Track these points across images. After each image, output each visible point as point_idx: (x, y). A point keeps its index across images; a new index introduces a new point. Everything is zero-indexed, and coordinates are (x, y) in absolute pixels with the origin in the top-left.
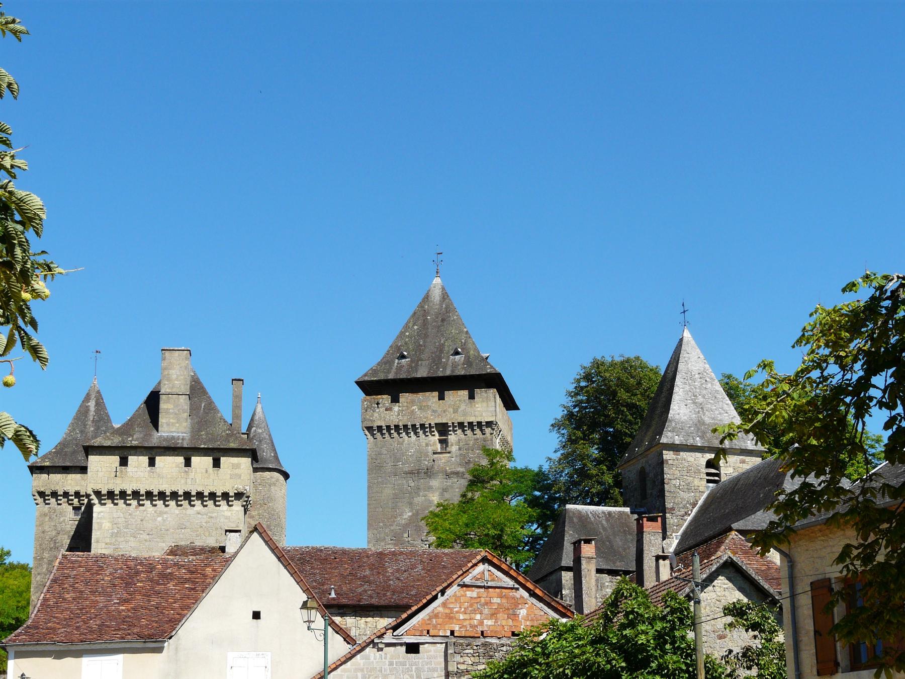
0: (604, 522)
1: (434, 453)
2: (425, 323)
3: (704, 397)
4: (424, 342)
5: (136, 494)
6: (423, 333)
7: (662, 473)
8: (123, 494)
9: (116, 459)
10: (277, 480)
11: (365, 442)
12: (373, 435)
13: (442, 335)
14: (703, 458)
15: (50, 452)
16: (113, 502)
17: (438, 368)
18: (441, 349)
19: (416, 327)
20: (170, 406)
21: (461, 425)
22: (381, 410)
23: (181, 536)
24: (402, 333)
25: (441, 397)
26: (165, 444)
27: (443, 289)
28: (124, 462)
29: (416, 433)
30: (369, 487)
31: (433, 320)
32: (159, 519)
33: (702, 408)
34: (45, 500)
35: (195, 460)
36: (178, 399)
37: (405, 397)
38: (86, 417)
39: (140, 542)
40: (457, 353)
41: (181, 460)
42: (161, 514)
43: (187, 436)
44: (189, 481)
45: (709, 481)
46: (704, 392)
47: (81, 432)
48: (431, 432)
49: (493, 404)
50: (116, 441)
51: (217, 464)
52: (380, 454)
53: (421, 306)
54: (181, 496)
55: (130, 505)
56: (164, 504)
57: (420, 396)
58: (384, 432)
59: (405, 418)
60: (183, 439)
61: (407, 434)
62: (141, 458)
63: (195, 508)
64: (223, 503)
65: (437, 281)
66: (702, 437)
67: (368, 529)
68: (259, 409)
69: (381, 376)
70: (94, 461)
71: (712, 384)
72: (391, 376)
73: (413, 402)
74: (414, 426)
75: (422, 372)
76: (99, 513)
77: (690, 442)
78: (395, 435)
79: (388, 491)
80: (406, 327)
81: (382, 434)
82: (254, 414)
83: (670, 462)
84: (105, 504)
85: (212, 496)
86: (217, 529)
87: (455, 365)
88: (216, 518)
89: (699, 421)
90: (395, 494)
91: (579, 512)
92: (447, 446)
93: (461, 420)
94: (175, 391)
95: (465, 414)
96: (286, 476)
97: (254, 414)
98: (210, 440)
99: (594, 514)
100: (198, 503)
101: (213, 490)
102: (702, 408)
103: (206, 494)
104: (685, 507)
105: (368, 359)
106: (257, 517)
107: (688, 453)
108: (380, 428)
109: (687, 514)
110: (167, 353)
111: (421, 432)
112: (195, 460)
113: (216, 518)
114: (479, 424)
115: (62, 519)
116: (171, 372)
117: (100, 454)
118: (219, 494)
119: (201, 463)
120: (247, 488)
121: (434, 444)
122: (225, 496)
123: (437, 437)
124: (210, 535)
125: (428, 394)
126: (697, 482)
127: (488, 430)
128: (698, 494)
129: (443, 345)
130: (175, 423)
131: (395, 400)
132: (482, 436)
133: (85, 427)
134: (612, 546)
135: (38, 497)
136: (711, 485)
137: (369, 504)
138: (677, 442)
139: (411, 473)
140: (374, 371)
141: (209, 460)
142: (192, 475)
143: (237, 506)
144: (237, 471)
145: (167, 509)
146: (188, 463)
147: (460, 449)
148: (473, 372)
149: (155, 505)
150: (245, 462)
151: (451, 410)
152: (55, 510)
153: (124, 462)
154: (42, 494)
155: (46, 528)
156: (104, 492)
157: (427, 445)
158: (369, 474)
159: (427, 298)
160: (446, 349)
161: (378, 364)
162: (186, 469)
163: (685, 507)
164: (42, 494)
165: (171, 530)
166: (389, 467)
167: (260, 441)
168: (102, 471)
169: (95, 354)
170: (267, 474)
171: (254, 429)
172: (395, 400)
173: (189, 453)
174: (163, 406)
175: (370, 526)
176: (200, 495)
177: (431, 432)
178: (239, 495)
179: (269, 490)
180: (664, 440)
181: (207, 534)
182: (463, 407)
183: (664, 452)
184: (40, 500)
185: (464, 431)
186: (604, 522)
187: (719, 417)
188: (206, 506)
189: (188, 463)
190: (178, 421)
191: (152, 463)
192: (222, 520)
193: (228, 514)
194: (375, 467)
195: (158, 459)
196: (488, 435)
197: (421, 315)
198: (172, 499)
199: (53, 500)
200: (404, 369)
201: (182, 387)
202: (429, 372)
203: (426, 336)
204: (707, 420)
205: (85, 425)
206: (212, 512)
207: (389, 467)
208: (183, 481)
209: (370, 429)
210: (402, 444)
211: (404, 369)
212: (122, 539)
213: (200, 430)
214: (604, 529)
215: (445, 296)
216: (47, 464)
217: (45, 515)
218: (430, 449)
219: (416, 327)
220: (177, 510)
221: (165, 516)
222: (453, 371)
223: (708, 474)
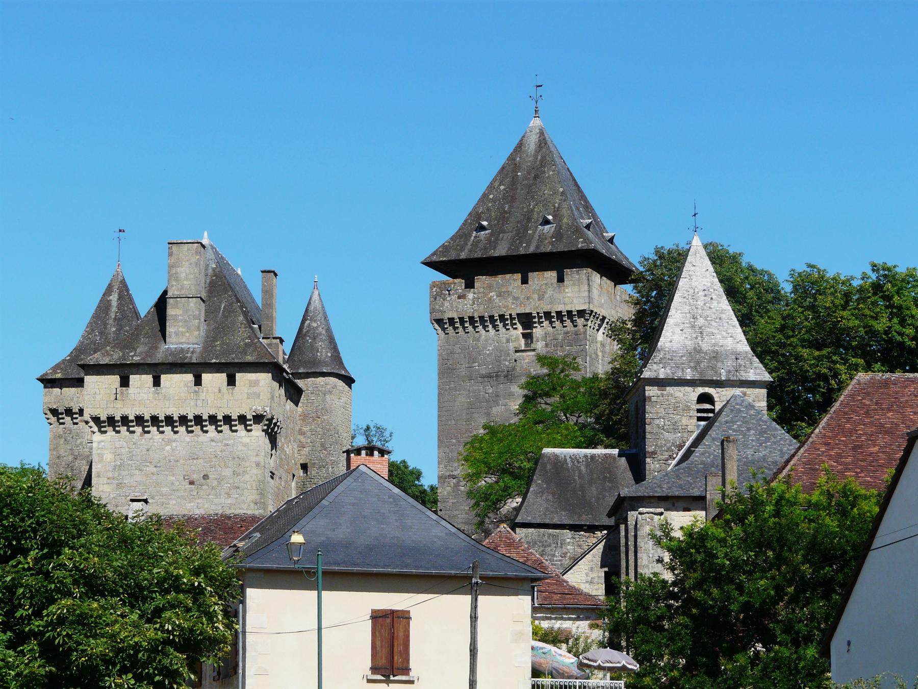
0: (583, 468)
1: (516, 351)
2: (514, 181)
3: (706, 318)
4: (511, 207)
5: (140, 420)
6: (510, 197)
7: (644, 412)
8: (125, 420)
9: (115, 379)
10: (335, 387)
11: (432, 338)
12: (444, 329)
13: (533, 197)
14: (693, 393)
15: (64, 360)
16: (114, 430)
17: (521, 243)
18: (528, 218)
19: (502, 187)
20: (179, 312)
21: (548, 315)
22: (453, 297)
23: (193, 468)
24: (485, 196)
25: (525, 281)
26: (170, 359)
27: (542, 133)
28: (125, 383)
29: (495, 327)
30: (440, 394)
31: (529, 174)
32: (168, 448)
33: (701, 333)
34: (58, 419)
35: (206, 377)
36: (188, 303)
37: (481, 281)
38: (107, 314)
39: (147, 475)
40: (546, 222)
41: (190, 377)
42: (170, 441)
43: (198, 348)
44: (200, 403)
45: (699, 419)
46: (708, 312)
47: (101, 333)
48: (513, 324)
49: (586, 287)
50: (115, 357)
51: (231, 381)
52: (452, 353)
53: (511, 158)
54: (191, 421)
55: (133, 432)
56: (173, 430)
57: (499, 279)
58: (458, 325)
59: (482, 308)
60: (193, 352)
61: (485, 327)
62: (144, 376)
63: (208, 435)
64: (240, 428)
65: (536, 123)
66: (694, 368)
67: (439, 447)
68: (316, 297)
69: (452, 256)
70: (90, 380)
71: (719, 303)
72: (463, 255)
73: (490, 287)
74: (491, 317)
75: (501, 250)
76: (99, 442)
77: (679, 374)
78: (470, 329)
79: (462, 399)
80: (491, 188)
81: (455, 328)
82: (309, 303)
83: (654, 399)
84: (105, 432)
85: (227, 419)
86: (234, 458)
87: (543, 238)
88: (233, 445)
89: (695, 349)
90: (470, 403)
91: (556, 456)
92: (532, 342)
93: (547, 308)
94: (184, 292)
95: (552, 301)
96: (349, 381)
97: (309, 303)
98: (224, 353)
99: (574, 458)
100: (211, 428)
101: (227, 412)
102: (701, 333)
103: (220, 417)
104: (669, 450)
105: (441, 228)
106: (309, 434)
107: (675, 388)
108: (451, 321)
109: (671, 457)
110: (174, 247)
111: (501, 325)
112: (206, 377)
113: (233, 445)
114: (569, 313)
115: (79, 441)
116: (179, 270)
117: (98, 374)
118: (234, 417)
119: (214, 380)
120: (267, 409)
121: (517, 339)
122: (242, 419)
123: (520, 330)
124: (226, 466)
125: (508, 276)
126: (685, 421)
127: (580, 321)
128: (685, 435)
129: (532, 210)
130: (186, 333)
131: (470, 285)
132: (573, 329)
133: (106, 328)
134: (584, 496)
135: (50, 416)
136: (703, 423)
137: (439, 416)
138: (661, 376)
139: (489, 376)
140: (445, 248)
141: (222, 377)
142: (202, 396)
143: (258, 431)
144: (255, 389)
145: (176, 436)
146: (198, 382)
147: (547, 345)
148: (562, 247)
149: (163, 432)
150: (265, 378)
151: (536, 296)
152: (71, 431)
153: (125, 383)
154: (54, 412)
155: (62, 452)
156: (103, 418)
157: (508, 341)
158: (440, 378)
159: (520, 146)
160: (535, 216)
161: (452, 239)
162: (196, 388)
163: (669, 450)
164: (54, 412)
165: (182, 461)
166: (463, 371)
167: (314, 338)
168: (98, 393)
169: (118, 234)
170: (321, 380)
171: (308, 322)
172: (470, 285)
173: (199, 369)
174: (170, 311)
175: (440, 442)
176: (213, 419)
177: (513, 324)
178: (258, 418)
179: (324, 400)
180: (647, 374)
181: (222, 464)
182: (550, 292)
183: (647, 388)
184: (53, 419)
185: (551, 323)
186: (583, 468)
187: (721, 342)
188: (221, 431)
189: (198, 382)
190: (189, 329)
191: (157, 383)
192: (240, 448)
193: (246, 440)
194: (447, 370)
195: (163, 377)
196: (580, 327)
197: (510, 171)
198: (181, 425)
199: (68, 419)
200: (481, 245)
201: (193, 288)
202: (509, 249)
203: (513, 199)
204: (705, 347)
205: (105, 325)
206: (229, 439)
207: (463, 371)
208: (192, 403)
209: (439, 322)
210: (478, 340)
211: (481, 245)
212: (127, 473)
213: (215, 339)
214: (581, 476)
215: (543, 142)
216: (59, 376)
217: (60, 437)
218: (512, 346)
219: (502, 187)
220: (188, 438)
221: (174, 444)
222: (537, 247)
223: (699, 411)
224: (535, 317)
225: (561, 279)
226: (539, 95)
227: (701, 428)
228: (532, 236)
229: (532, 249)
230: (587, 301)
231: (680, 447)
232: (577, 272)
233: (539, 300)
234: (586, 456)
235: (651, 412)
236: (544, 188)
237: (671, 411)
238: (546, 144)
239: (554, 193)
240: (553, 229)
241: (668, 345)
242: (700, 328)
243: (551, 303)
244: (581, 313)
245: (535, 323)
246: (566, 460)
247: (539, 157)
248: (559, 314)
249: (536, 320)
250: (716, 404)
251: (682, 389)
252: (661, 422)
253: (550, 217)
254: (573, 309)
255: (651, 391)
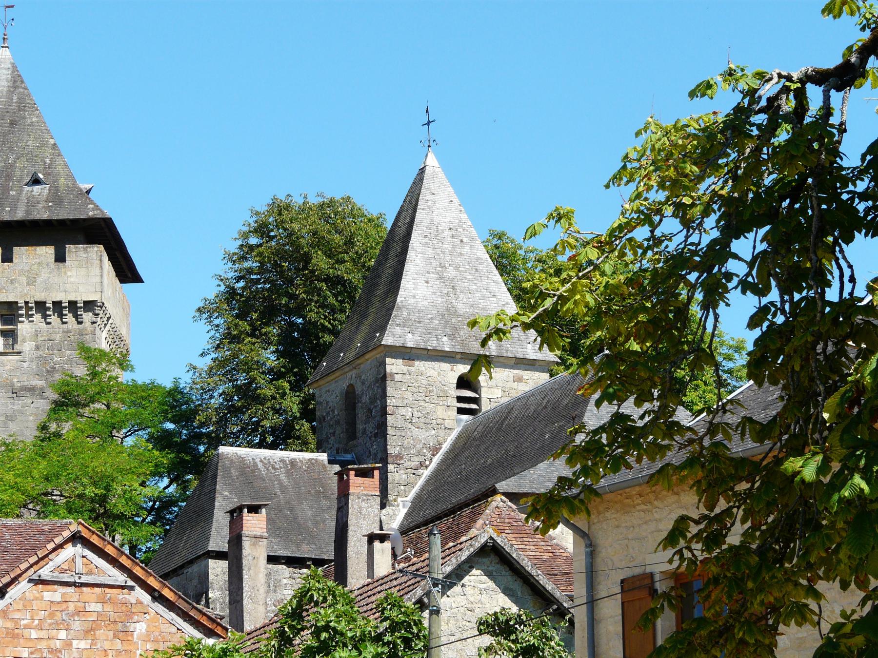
0: (283, 477)
3: (457, 268)
13: (11, 149)
21: (41, 306)
33: (453, 288)
45: (461, 411)
66: (452, 337)
77: (432, 344)
83: (397, 377)
91: (242, 459)
93: (40, 297)
99: (267, 463)
102: (453, 288)
107: (428, 364)
114: (73, 305)
126: (441, 412)
127: (87, 317)
128: (442, 433)
129: (12, 166)
134: (295, 518)
138: (410, 344)
147: (37, 348)
151: (24, 279)
160: (18, 173)
180: (388, 340)
182: (44, 275)
185: (45, 317)
186: (283, 477)
196: (87, 324)
214: (283, 488)
222: (28, 212)
223: (460, 399)
224: (21, 308)
225: (60, 258)
226: (9, 19)
227: (463, 424)
228: (17, 200)
229: (20, 215)
230: (98, 289)
231: (435, 450)
232: (85, 250)
233: (28, 284)
234: (282, 461)
235: (395, 396)
236: (26, 137)
237: (421, 397)
238: (22, 82)
239: (42, 146)
240: (46, 191)
241: (412, 301)
242: (452, 281)
243: (46, 289)
244: (89, 305)
245: (22, 315)
246: (255, 465)
247: (15, 98)
248: (57, 305)
249: (23, 312)
250: (483, 390)
251: (436, 365)
252: (408, 412)
253: (41, 176)
254: (78, 299)
255: (393, 366)
